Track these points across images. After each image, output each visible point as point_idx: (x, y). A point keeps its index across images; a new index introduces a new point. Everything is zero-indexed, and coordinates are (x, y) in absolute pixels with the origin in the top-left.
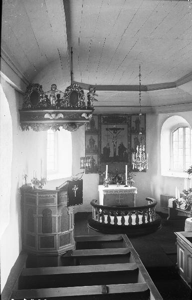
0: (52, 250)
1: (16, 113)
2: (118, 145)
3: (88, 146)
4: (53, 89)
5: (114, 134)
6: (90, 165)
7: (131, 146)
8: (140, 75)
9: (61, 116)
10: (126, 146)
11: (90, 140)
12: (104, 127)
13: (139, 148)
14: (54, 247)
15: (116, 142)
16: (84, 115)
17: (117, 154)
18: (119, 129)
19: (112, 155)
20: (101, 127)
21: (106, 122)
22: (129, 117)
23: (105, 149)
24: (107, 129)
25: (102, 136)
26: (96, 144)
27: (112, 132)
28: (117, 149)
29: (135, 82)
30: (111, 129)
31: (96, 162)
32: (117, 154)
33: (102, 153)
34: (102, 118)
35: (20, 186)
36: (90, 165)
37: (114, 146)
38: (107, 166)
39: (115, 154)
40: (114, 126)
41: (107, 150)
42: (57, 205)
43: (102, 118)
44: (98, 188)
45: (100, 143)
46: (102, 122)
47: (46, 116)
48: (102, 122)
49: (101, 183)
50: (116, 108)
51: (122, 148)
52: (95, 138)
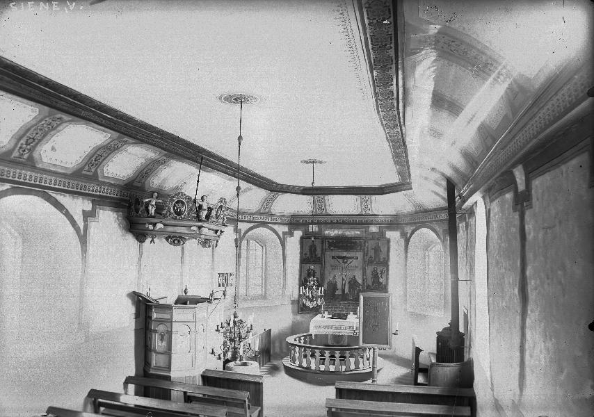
12: (329, 254)
19: (338, 292)
24: (333, 257)
27: (341, 261)
37: (343, 280)
39: (343, 291)
43: (327, 243)
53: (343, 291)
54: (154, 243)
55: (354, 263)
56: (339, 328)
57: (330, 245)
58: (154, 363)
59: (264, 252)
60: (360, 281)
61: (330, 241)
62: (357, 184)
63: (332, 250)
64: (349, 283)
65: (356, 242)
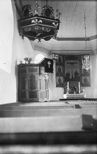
0: (35, 99)
1: (16, 23)
2: (74, 72)
3: (57, 72)
4: (37, 6)
5: (72, 66)
6: (57, 58)
7: (81, 73)
8: (85, 18)
9: (41, 21)
10: (79, 72)
11: (58, 68)
12: (66, 62)
13: (86, 57)
14: (37, 98)
15: (73, 70)
16: (54, 23)
17: (74, 77)
18: (74, 63)
19: (71, 77)
20: (64, 62)
21: (67, 59)
22: (80, 56)
23: (67, 74)
24: (68, 63)
25: (65, 67)
26: (62, 71)
27: (71, 64)
28: (74, 74)
29: (83, 36)
30: (70, 63)
31: (62, 81)
32: (74, 77)
33: (65, 76)
34: (65, 57)
35: (19, 63)
36: (57, 58)
37: (72, 72)
38: (68, 82)
39: (72, 77)
40: (72, 61)
41: (68, 75)
42: (38, 73)
43: (65, 57)
44: (63, 96)
45: (64, 71)
46: (65, 59)
47: (33, 21)
48: (65, 59)
49: (65, 93)
50: (72, 51)
51: (76, 73)
52: (61, 67)
53: (72, 77)
54: (40, 41)
55: (76, 65)
56: (73, 96)
57: (66, 58)
58: (28, 63)
59: (21, 4)
60: (79, 73)
61: (66, 56)
62: (81, 37)
63: (67, 60)
64: (74, 73)
65: (76, 57)
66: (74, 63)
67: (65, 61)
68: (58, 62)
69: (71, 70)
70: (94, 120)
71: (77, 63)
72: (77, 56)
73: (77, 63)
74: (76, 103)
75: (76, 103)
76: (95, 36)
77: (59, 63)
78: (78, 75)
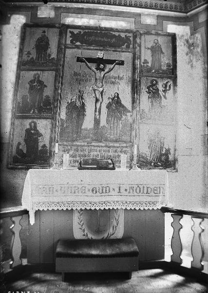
18: (111, 62)
21: (78, 43)
28: (104, 110)
30: (91, 60)
34: (69, 35)
37: (97, 100)
40: (100, 55)
43: (69, 35)
46: (68, 42)
53: (97, 122)
57: (75, 38)
63: (78, 47)
66: (111, 62)
67: (69, 52)
68: (34, 55)
69: (95, 90)
70: (184, 280)
71: (122, 63)
72: (123, 35)
73: (122, 63)
74: (110, 8)
75: (102, 7)
76: (73, 235)
77: (38, 58)
78: (124, 117)
